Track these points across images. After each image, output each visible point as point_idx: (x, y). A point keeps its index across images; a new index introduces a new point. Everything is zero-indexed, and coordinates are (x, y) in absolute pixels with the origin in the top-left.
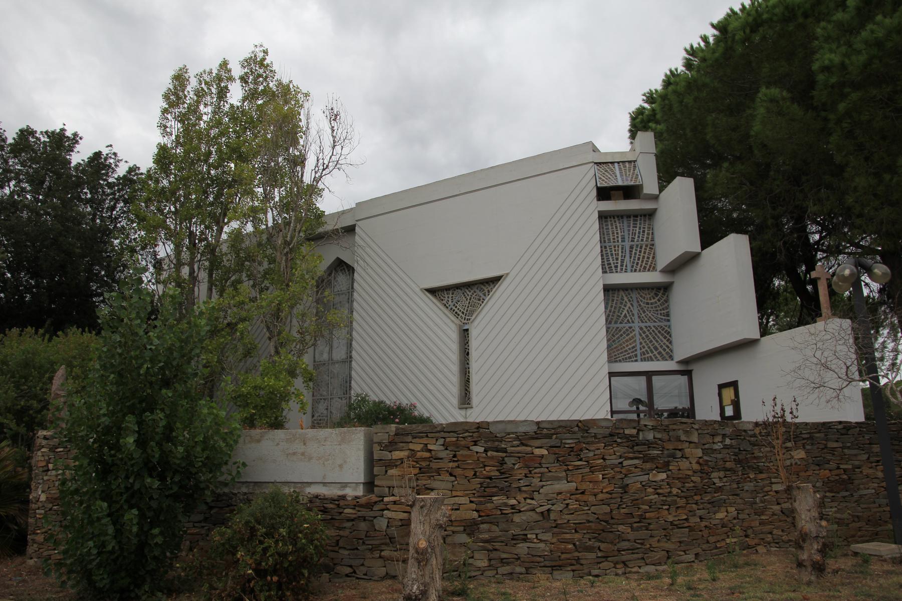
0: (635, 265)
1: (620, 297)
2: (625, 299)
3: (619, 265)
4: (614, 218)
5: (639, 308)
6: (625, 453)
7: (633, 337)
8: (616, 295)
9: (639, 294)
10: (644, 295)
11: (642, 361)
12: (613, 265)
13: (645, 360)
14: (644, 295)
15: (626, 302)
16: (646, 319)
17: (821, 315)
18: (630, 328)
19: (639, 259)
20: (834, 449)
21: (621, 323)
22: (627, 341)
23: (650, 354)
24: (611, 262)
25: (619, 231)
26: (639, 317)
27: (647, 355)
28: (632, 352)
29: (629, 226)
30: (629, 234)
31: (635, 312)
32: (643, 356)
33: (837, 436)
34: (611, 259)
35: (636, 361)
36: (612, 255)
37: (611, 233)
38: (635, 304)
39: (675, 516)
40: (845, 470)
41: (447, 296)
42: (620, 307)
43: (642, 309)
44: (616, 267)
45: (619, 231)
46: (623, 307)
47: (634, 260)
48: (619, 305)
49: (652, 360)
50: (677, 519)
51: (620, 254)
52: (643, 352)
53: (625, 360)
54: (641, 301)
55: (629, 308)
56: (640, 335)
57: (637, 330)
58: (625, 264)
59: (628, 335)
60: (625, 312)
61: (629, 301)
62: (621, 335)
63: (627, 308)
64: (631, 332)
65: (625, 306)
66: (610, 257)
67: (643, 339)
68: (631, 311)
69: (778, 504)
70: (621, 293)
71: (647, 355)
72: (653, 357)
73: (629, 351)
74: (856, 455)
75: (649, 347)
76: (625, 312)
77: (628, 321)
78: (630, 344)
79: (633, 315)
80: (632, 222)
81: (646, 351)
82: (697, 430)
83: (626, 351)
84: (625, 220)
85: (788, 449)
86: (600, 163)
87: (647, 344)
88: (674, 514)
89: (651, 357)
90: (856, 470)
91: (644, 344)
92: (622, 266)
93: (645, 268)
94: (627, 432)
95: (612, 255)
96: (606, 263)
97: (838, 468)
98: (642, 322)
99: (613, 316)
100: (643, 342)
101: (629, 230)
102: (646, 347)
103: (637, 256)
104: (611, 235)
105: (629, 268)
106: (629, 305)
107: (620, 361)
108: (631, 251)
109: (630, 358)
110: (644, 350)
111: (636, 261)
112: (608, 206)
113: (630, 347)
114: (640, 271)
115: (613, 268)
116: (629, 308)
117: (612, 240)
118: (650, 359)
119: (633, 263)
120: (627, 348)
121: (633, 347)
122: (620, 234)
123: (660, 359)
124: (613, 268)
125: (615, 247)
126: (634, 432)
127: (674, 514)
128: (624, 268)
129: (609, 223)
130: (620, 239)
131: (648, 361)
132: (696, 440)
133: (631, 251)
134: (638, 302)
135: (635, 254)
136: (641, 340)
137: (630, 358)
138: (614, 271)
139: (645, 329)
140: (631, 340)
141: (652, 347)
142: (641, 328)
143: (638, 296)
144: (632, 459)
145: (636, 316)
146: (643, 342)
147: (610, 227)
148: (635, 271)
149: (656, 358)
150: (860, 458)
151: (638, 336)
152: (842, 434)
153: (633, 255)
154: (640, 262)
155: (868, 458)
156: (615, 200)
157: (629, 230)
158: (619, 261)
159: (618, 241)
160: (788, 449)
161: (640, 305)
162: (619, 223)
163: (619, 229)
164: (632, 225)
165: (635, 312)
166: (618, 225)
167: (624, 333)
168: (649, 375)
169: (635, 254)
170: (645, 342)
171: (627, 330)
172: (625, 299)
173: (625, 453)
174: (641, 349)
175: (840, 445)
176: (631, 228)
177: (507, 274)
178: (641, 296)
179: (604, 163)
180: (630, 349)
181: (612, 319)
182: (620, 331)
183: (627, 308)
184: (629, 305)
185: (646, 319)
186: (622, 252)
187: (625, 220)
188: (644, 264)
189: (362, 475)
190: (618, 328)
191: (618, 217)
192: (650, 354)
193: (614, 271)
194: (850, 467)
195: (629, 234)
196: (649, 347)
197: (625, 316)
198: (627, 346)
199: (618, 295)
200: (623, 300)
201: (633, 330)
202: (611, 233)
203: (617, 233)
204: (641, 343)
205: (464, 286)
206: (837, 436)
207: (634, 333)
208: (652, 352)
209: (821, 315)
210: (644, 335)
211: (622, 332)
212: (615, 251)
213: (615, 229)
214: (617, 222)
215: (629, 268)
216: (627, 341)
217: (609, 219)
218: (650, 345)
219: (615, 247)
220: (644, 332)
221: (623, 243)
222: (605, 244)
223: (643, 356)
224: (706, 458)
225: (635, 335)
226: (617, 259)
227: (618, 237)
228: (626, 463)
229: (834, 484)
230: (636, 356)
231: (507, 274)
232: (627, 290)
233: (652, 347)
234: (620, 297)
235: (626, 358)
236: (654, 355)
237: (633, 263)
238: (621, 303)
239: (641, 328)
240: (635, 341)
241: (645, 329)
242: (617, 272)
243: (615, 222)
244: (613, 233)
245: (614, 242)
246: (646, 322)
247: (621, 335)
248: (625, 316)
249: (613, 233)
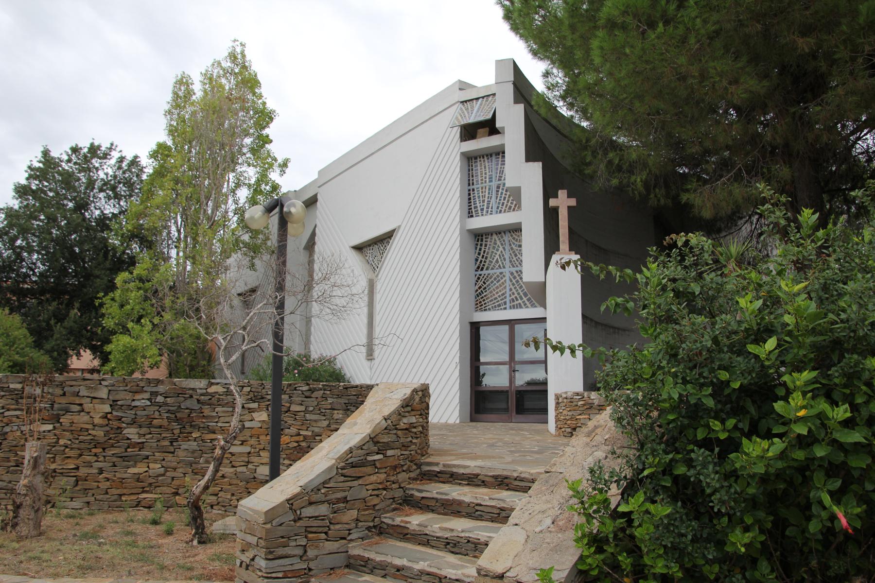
0: (500, 206)
1: (493, 241)
2: (498, 243)
3: (485, 207)
4: (483, 158)
5: (511, 252)
6: (8, 405)
7: (503, 283)
8: (489, 240)
9: (512, 236)
10: (516, 237)
11: (511, 308)
12: (479, 209)
13: (514, 308)
14: (516, 237)
15: (498, 246)
16: (517, 263)
17: (559, 250)
18: (501, 273)
19: (504, 199)
20: (295, 413)
21: (492, 269)
22: (497, 288)
23: (520, 301)
24: (478, 205)
25: (487, 171)
26: (511, 261)
27: (517, 302)
28: (501, 300)
29: (497, 164)
30: (497, 173)
31: (507, 256)
32: (512, 304)
33: (300, 399)
34: (478, 202)
35: (505, 309)
36: (479, 197)
37: (479, 174)
38: (507, 247)
39: (60, 465)
40: (305, 437)
41: (369, 251)
42: (493, 252)
43: (514, 252)
44: (482, 210)
45: (487, 171)
46: (495, 251)
47: (500, 200)
48: (491, 250)
49: (521, 307)
50: (60, 467)
51: (487, 195)
52: (513, 299)
53: (494, 308)
54: (514, 244)
55: (502, 252)
56: (511, 281)
57: (508, 275)
58: (491, 205)
59: (499, 281)
60: (497, 256)
61: (502, 244)
62: (492, 282)
63: (499, 253)
64: (502, 278)
65: (497, 250)
66: (477, 200)
67: (513, 284)
68: (503, 255)
69: (233, 467)
70: (495, 236)
71: (517, 302)
72: (522, 304)
73: (499, 299)
74: (315, 421)
75: (519, 294)
76: (497, 256)
77: (499, 266)
78: (500, 291)
79: (505, 259)
80: (500, 159)
81: (516, 297)
82: (106, 386)
83: (496, 298)
84: (494, 157)
85: (251, 411)
86: (466, 101)
87: (517, 290)
88: (59, 463)
89: (520, 304)
90: (316, 438)
91: (514, 290)
92: (488, 208)
93: (510, 207)
94: (12, 386)
95: (479, 197)
96: (473, 207)
97: (299, 435)
98: (514, 266)
99: (485, 262)
100: (513, 288)
101: (497, 169)
102: (516, 293)
103: (503, 196)
104: (480, 176)
105: (494, 210)
106: (501, 249)
107: (489, 309)
108: (498, 191)
109: (499, 306)
110: (513, 297)
111: (502, 201)
112: (472, 146)
113: (500, 294)
114: (505, 212)
115: (480, 212)
116: (502, 252)
117: (480, 182)
118: (519, 306)
119: (499, 203)
120: (496, 296)
121: (503, 294)
122: (488, 174)
123: (529, 306)
124: (480, 212)
125: (482, 188)
126: (19, 386)
127: (59, 463)
128: (490, 210)
129: (479, 163)
130: (488, 180)
131: (517, 308)
132: (105, 396)
133: (498, 191)
134: (510, 245)
135: (502, 193)
136: (511, 286)
137: (499, 306)
138: (480, 214)
139: (516, 274)
140: (501, 286)
141: (521, 294)
142: (512, 274)
143: (511, 238)
144: (15, 410)
145: (508, 260)
146: (513, 288)
147: (479, 168)
148: (501, 211)
149: (525, 304)
150: (319, 424)
151: (508, 281)
152: (306, 397)
153: (499, 195)
154: (506, 202)
155: (328, 426)
156: (480, 138)
157: (497, 169)
158: (485, 204)
159: (486, 182)
160: (251, 411)
161: (512, 249)
162: (488, 162)
163: (487, 169)
164: (500, 162)
165: (507, 256)
166: (487, 164)
167: (495, 279)
168: (511, 323)
169: (502, 193)
170: (515, 288)
171: (498, 276)
172: (498, 243)
173: (8, 405)
174: (510, 296)
175: (302, 408)
176: (500, 166)
177: (399, 227)
178: (514, 238)
179: (469, 101)
180: (499, 296)
181: (484, 265)
182: (491, 277)
183: (499, 253)
184: (501, 249)
185: (517, 263)
186: (489, 193)
187: (494, 157)
188: (509, 204)
189: (457, 413)
190: (489, 274)
191: (487, 156)
192: (520, 301)
193: (480, 214)
194: (310, 433)
195: (497, 173)
196: (519, 294)
197: (497, 261)
198: (497, 293)
199: (491, 239)
200: (495, 244)
201: (504, 276)
202: (479, 174)
203: (486, 174)
204: (511, 290)
205: (379, 241)
206: (300, 399)
207: (504, 279)
208: (521, 298)
209: (559, 250)
210: (514, 281)
211: (492, 279)
212: (482, 192)
213: (483, 170)
214: (486, 161)
215: (494, 210)
216: (497, 288)
217: (478, 159)
218: (520, 291)
219: (482, 188)
220: (515, 278)
221: (491, 184)
222: (473, 187)
223: (512, 304)
224: (115, 413)
225: (505, 281)
226: (484, 201)
227: (485, 178)
228: (7, 414)
229: (292, 451)
230: (505, 303)
231: (399, 227)
232: (500, 233)
233: (521, 294)
234: (493, 241)
235: (495, 307)
236: (524, 302)
237: (499, 203)
238: (494, 248)
239: (512, 274)
240: (505, 287)
241: (516, 274)
242: (482, 215)
243: (484, 161)
244: (482, 174)
245: (482, 183)
246: (517, 266)
247: (492, 282)
248: (497, 261)
249: (482, 174)
